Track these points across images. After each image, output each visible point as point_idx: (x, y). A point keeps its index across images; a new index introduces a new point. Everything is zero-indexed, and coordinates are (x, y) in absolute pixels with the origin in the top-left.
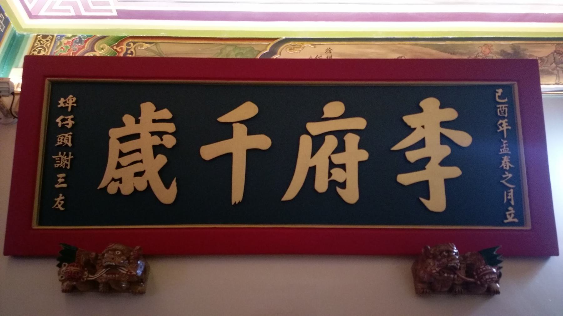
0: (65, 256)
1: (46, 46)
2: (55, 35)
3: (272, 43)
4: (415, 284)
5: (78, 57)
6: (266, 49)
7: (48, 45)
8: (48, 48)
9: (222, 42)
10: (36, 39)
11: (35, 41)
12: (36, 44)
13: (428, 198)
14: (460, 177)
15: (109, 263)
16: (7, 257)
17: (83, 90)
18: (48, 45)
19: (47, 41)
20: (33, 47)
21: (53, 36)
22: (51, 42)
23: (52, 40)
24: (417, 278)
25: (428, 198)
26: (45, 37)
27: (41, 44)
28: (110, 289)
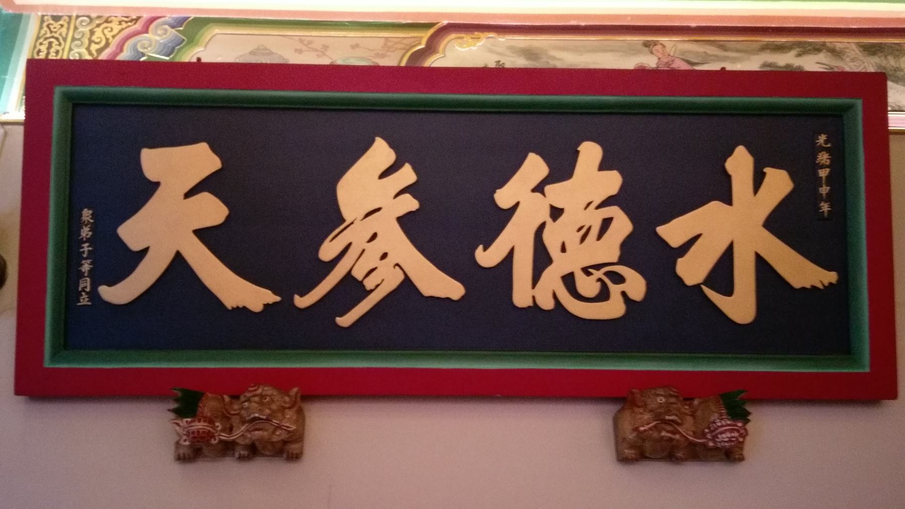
0: (187, 407)
1: (60, 34)
2: (74, 14)
3: (431, 31)
4: (304, 429)
5: (119, 62)
6: (420, 44)
7: (64, 34)
8: (65, 39)
9: (435, 109)
10: (42, 21)
11: (41, 28)
12: (43, 32)
13: (485, 249)
14: (533, 151)
15: (257, 415)
16: (21, 398)
17: (98, 118)
18: (64, 34)
19: (62, 26)
20: (38, 38)
21: (70, 17)
22: (68, 29)
23: (69, 23)
24: (619, 439)
25: (485, 249)
26: (56, 18)
27: (51, 32)
28: (697, 452)
